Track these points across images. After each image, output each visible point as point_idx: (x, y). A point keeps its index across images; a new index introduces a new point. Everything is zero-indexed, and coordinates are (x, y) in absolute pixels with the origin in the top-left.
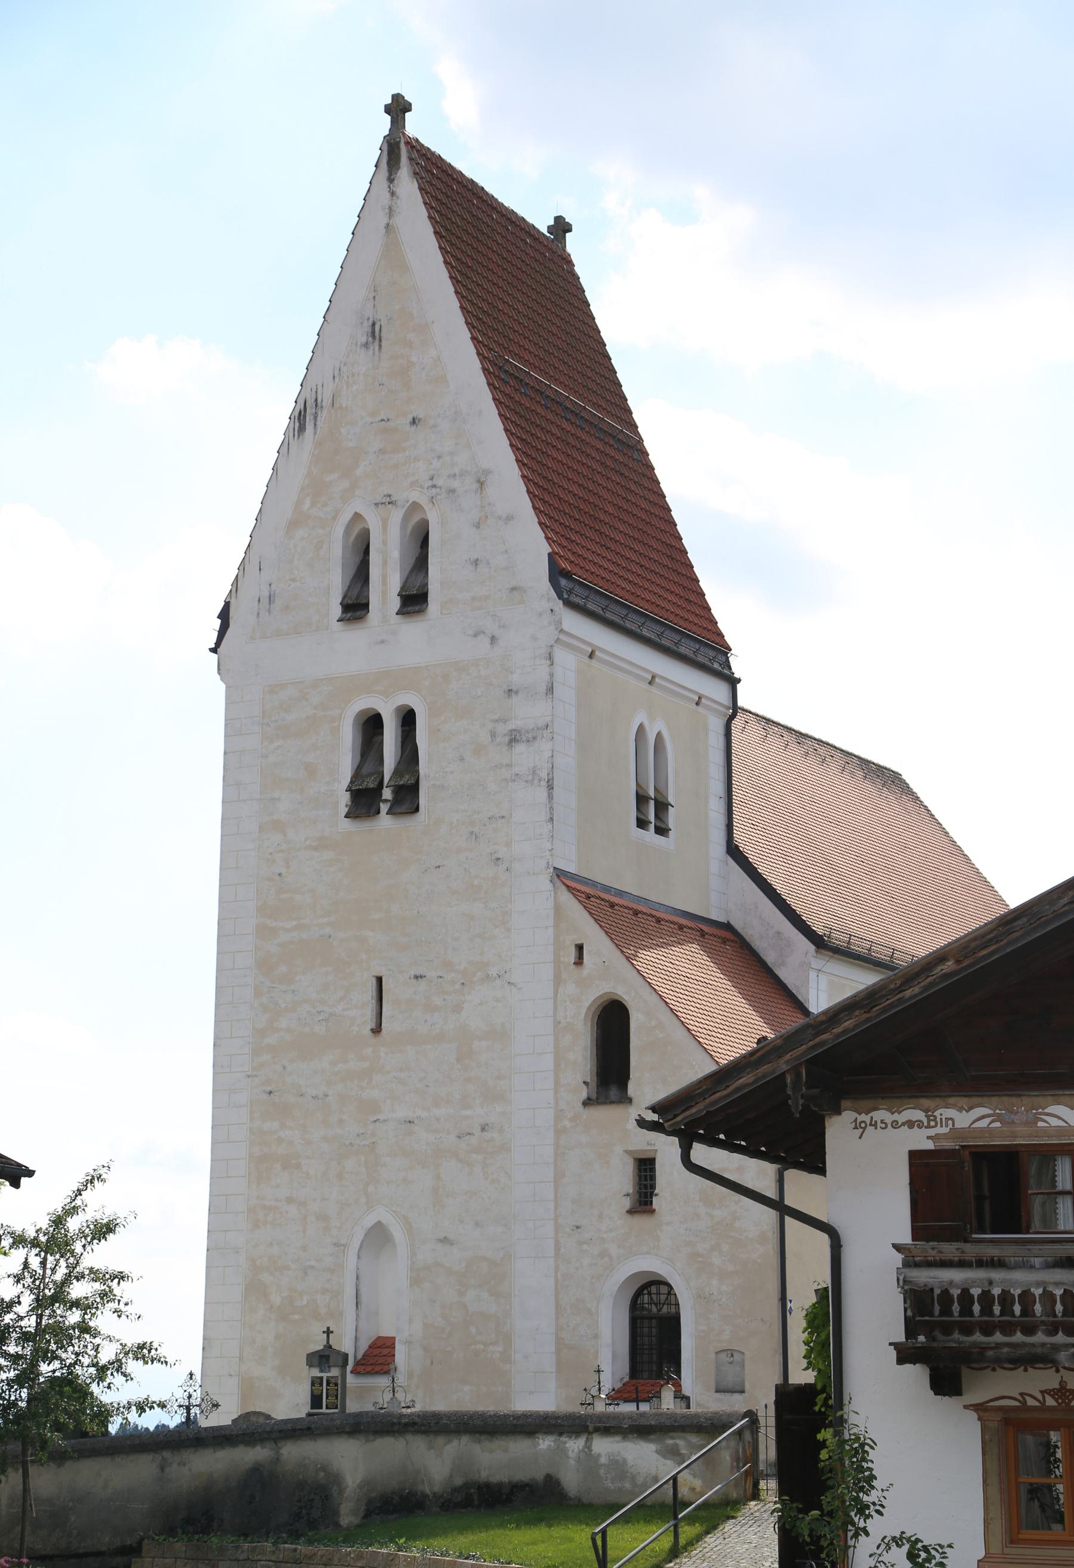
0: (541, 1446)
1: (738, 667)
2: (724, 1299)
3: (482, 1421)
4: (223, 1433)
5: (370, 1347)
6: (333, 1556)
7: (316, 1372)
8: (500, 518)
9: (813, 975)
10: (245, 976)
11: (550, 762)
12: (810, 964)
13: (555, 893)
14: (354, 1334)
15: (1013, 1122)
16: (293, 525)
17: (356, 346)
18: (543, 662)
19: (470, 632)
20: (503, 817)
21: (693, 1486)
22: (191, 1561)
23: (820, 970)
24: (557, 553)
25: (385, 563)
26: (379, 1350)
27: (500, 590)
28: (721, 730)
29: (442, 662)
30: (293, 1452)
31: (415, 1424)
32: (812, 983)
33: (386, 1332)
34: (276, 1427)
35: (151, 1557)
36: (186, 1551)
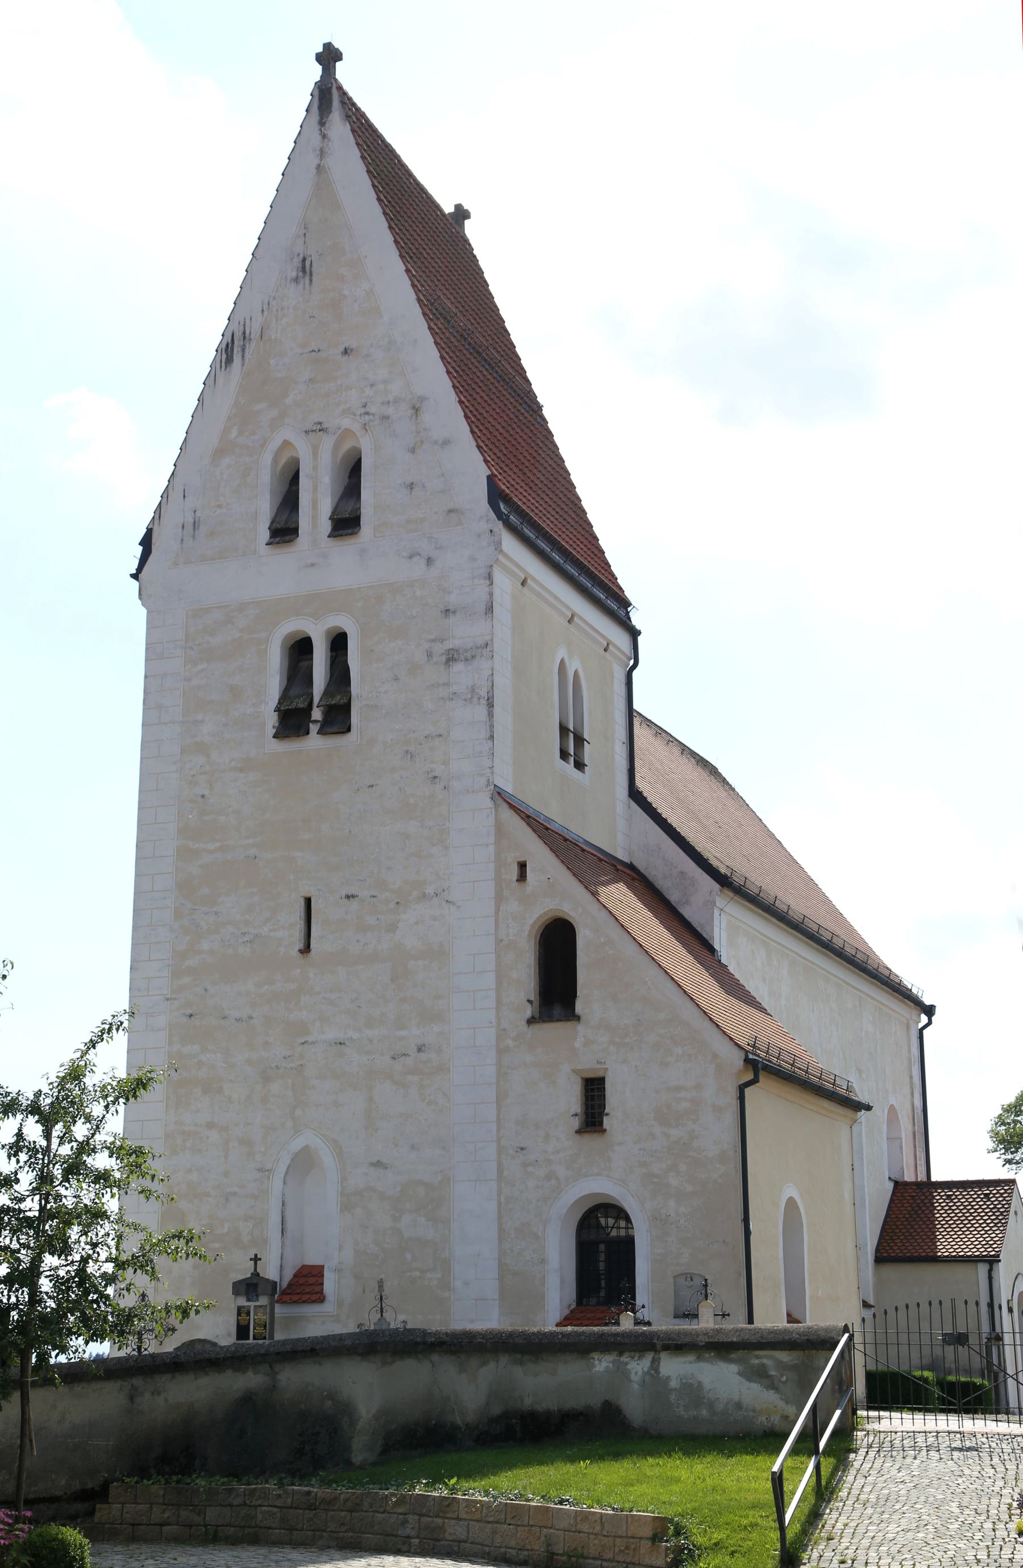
0: (597, 1369)
1: (637, 619)
2: (682, 1221)
3: (524, 1339)
5: (295, 1276)
6: (362, 1500)
7: (242, 1301)
8: (436, 442)
9: (716, 913)
10: (165, 898)
11: (490, 680)
12: (715, 902)
13: (496, 810)
14: (280, 1263)
16: (219, 453)
17: (286, 281)
18: (482, 582)
19: (405, 554)
20: (440, 736)
21: (786, 1413)
22: (171, 1507)
23: (722, 910)
25: (315, 489)
27: (436, 513)
29: (375, 584)
32: (716, 922)
33: (312, 1260)
34: (272, 1349)
35: (120, 1503)
36: (164, 1495)
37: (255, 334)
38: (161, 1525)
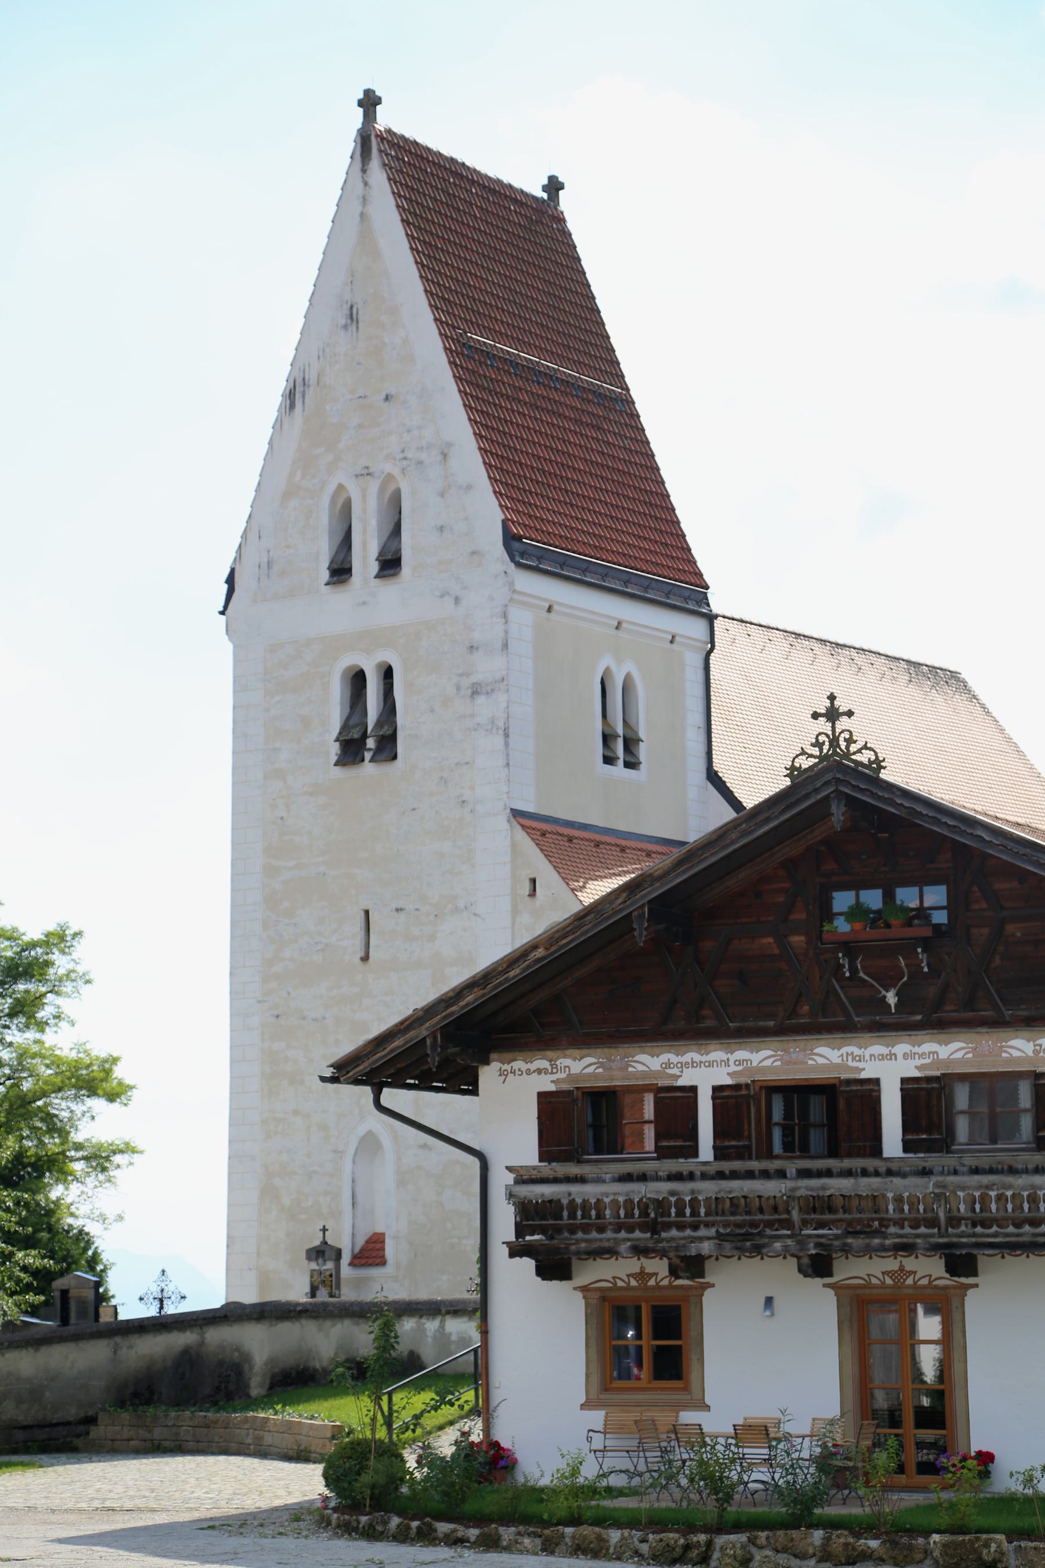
4: (161, 1321)
5: (367, 1242)
7: (314, 1266)
13: (512, 832)
15: (611, 1068)
24: (509, 520)
25: (365, 531)
26: (374, 1245)
28: (700, 664)
30: (216, 1336)
31: (307, 1311)
33: (379, 1230)
37: (313, 381)
38: (129, 1440)
